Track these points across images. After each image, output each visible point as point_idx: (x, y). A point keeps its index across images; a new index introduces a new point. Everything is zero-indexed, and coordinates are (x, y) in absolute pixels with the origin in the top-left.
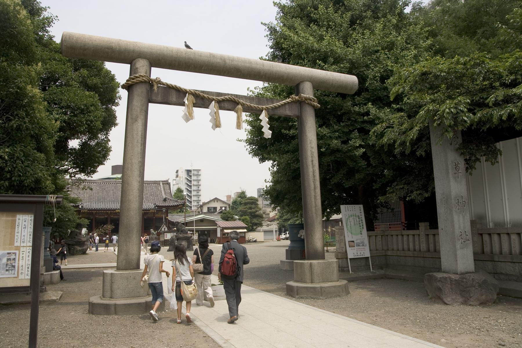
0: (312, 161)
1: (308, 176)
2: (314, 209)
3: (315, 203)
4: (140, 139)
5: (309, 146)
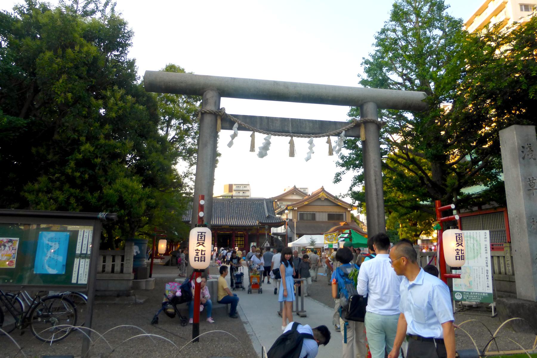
3: (378, 221)
5: (372, 165)
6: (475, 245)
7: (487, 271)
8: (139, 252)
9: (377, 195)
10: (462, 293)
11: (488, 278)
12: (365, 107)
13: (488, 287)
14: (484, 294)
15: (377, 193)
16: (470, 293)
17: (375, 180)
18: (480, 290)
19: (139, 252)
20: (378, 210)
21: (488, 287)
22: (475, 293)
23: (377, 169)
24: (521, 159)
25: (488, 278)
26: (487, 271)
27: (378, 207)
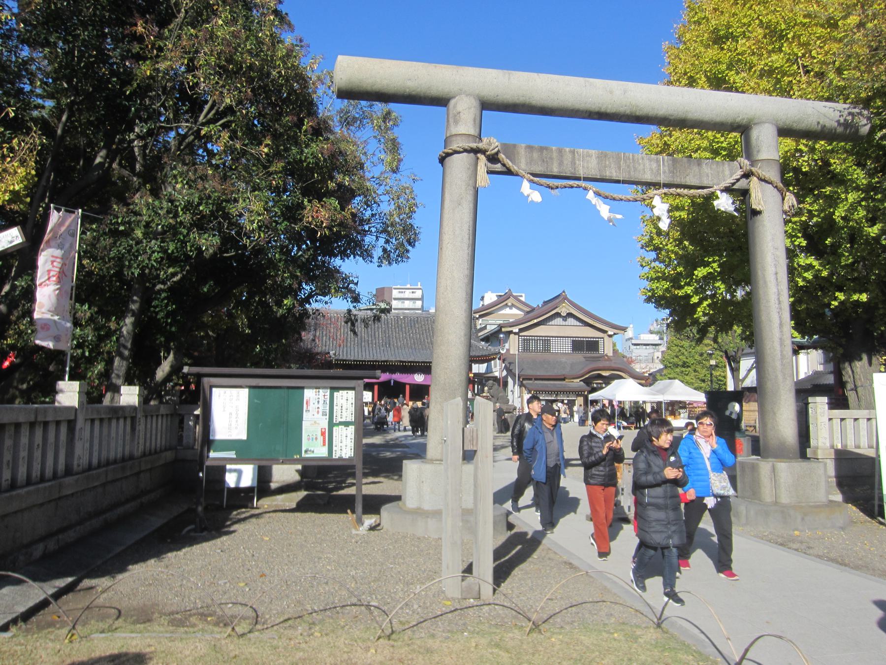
0: (776, 274)
1: (768, 301)
2: (778, 364)
3: (781, 352)
4: (467, 237)
5: (770, 244)
8: (307, 306)
12: (755, 133)
15: (779, 299)
17: (776, 274)
20: (781, 332)
23: (778, 253)
26: (231, 414)
27: (781, 325)
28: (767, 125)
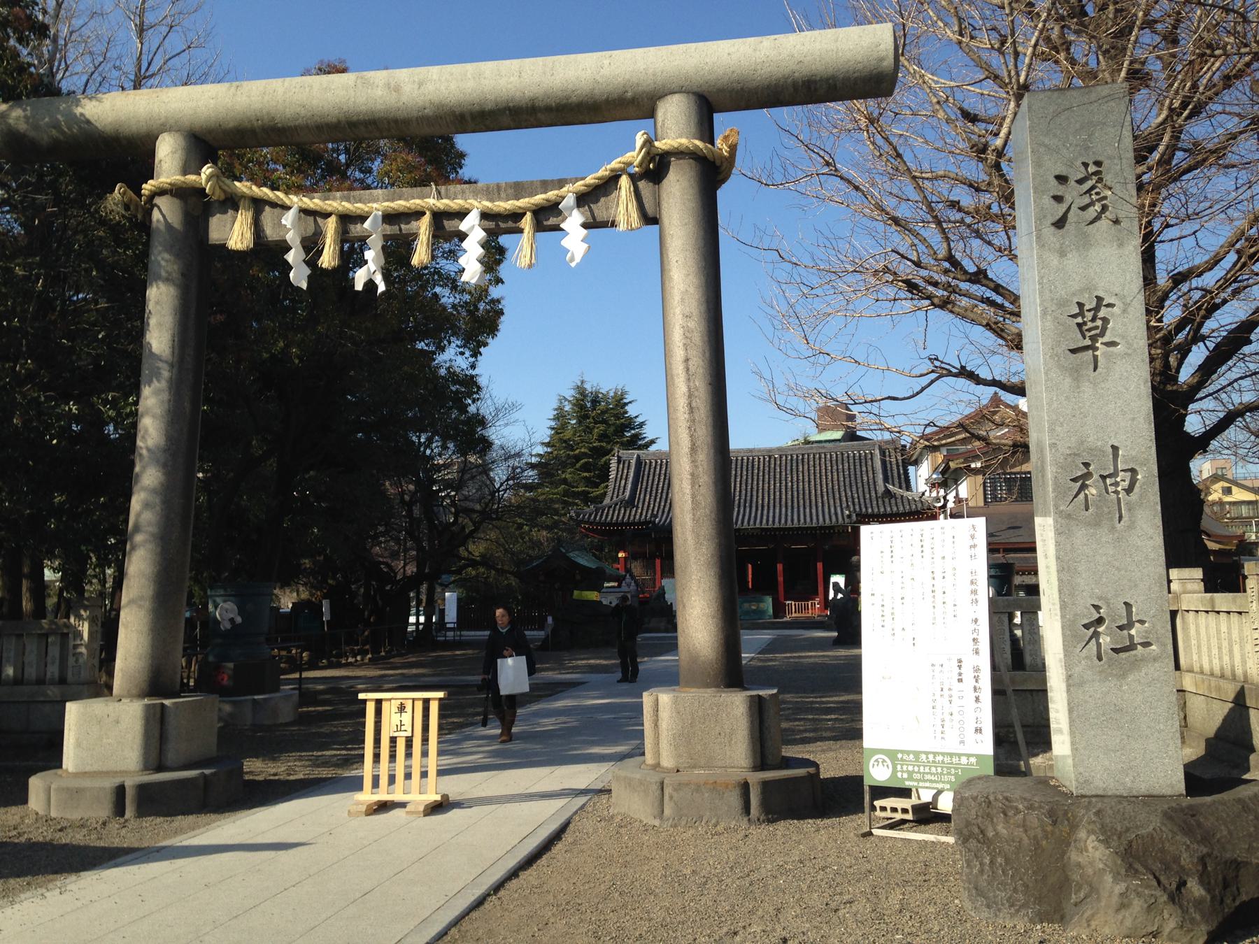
3: (693, 496)
5: (678, 311)
6: (938, 575)
7: (977, 670)
9: (691, 410)
10: (892, 754)
11: (977, 699)
13: (979, 730)
14: (964, 760)
15: (690, 404)
16: (917, 754)
17: (687, 360)
18: (952, 745)
19: (239, 620)
21: (979, 730)
22: (935, 754)
24: (1049, 231)
25: (977, 699)
26: (977, 670)
27: (693, 449)
28: (676, 98)
